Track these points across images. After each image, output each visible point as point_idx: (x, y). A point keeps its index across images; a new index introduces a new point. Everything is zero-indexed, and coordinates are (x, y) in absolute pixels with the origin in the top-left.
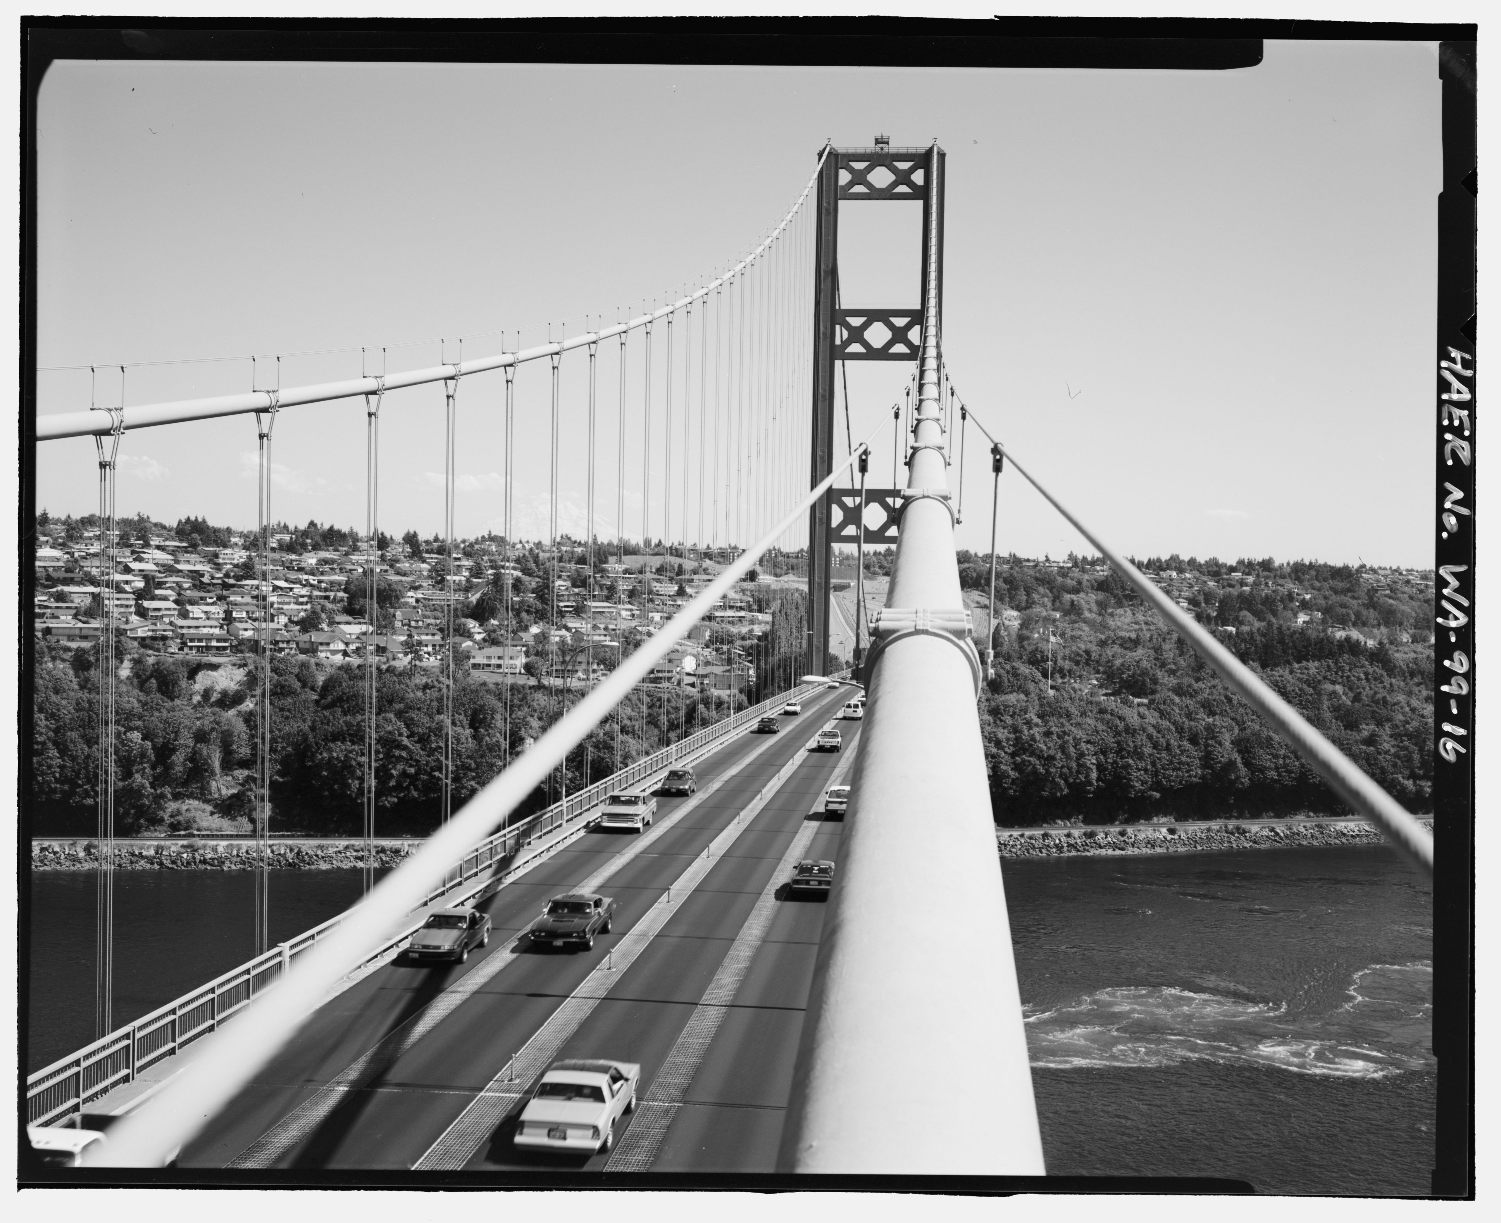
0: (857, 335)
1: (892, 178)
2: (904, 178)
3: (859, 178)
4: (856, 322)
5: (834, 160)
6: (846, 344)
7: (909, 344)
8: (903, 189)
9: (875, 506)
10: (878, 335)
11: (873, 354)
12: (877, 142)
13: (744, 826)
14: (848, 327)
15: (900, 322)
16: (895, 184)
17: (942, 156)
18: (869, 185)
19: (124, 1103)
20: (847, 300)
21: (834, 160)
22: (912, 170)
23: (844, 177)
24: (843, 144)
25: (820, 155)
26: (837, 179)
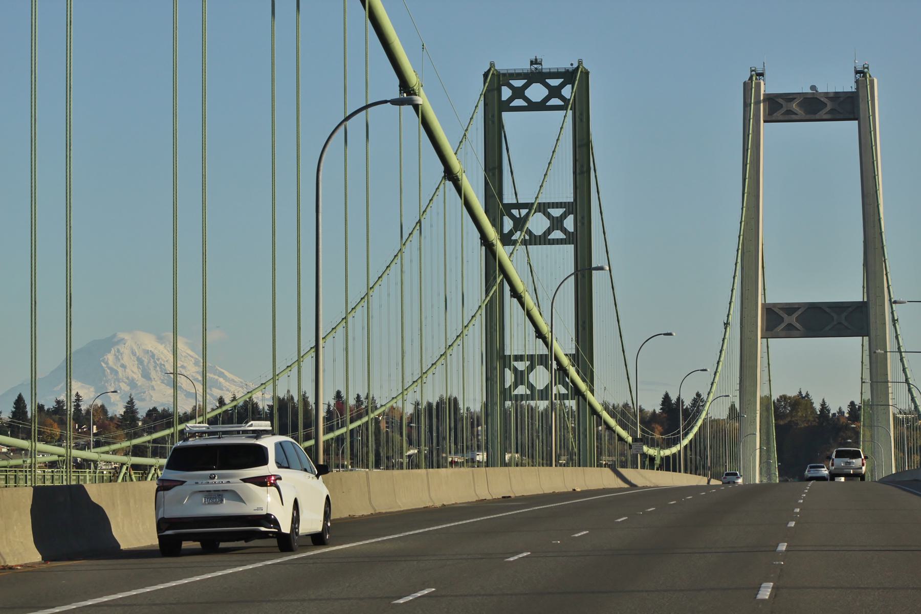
0: (557, 223)
2: (555, 92)
3: (519, 93)
4: (557, 234)
5: (495, 80)
6: (564, 216)
7: (564, 231)
8: (521, 366)
9: (540, 369)
10: (538, 224)
11: (533, 106)
12: (532, 63)
13: (483, 493)
14: (564, 231)
15: (556, 212)
16: (549, 231)
17: (586, 73)
18: (526, 99)
19: (163, 583)
21: (495, 80)
22: (562, 86)
23: (506, 93)
24: (503, 66)
25: (486, 75)
26: (500, 94)
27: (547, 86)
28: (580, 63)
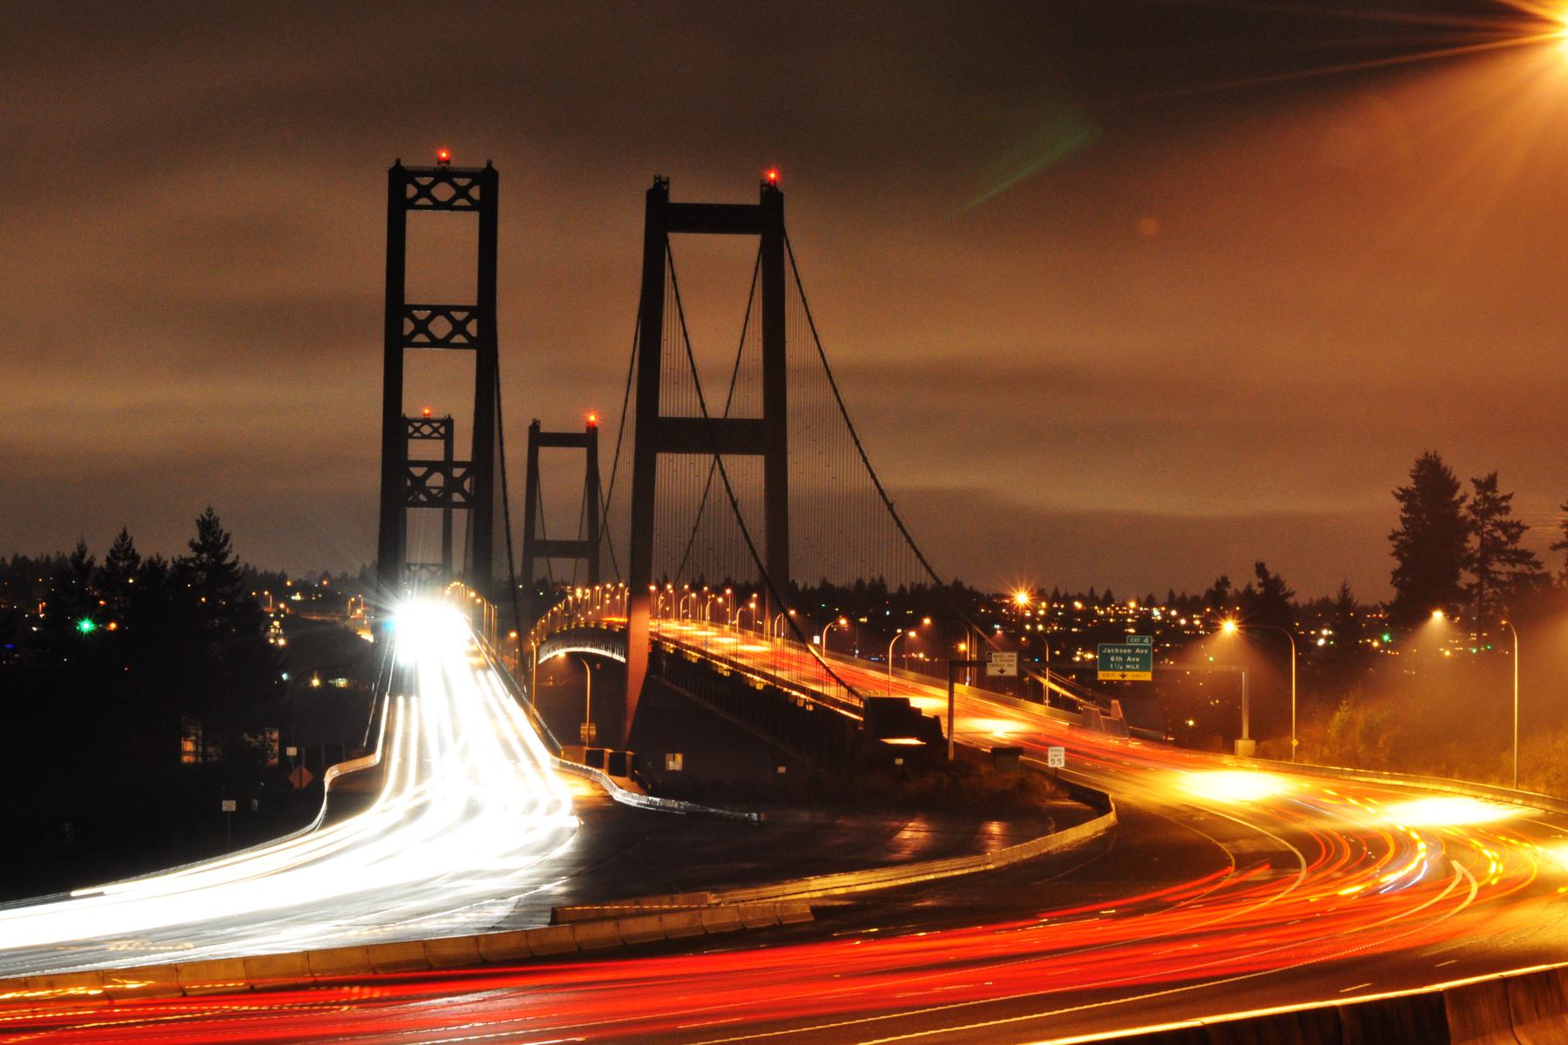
0: (422, 327)
1: (453, 192)
3: (424, 191)
14: (413, 319)
20: (410, 298)
22: (470, 186)
27: (454, 185)
28: (489, 163)
